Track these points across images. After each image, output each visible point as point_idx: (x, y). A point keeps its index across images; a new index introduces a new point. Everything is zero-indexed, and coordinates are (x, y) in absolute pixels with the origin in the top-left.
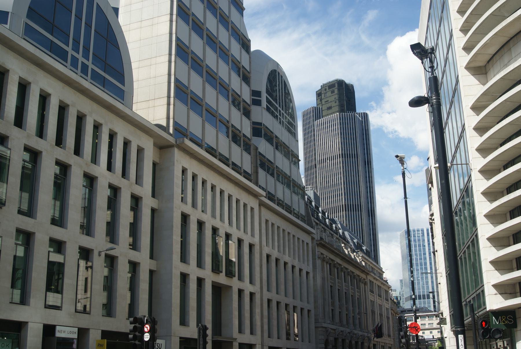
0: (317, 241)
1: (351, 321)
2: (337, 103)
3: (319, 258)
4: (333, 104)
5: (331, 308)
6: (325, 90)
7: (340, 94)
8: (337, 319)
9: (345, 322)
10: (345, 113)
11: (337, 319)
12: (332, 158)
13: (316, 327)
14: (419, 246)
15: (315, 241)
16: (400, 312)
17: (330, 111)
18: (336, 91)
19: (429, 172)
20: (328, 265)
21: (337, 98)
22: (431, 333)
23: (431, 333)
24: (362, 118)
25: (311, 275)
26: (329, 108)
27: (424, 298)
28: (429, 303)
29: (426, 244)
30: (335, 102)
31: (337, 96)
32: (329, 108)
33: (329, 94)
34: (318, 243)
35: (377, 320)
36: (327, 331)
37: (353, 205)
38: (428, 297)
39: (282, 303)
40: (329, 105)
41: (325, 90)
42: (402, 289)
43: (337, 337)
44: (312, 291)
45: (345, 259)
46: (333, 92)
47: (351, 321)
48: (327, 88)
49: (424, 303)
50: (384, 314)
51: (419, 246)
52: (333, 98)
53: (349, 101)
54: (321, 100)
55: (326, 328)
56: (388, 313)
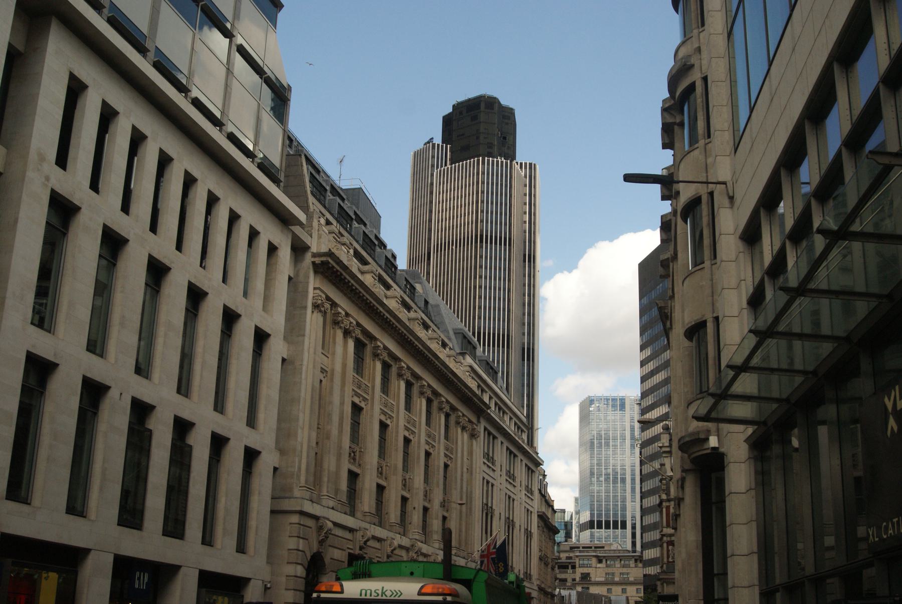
0: (314, 255)
1: (416, 518)
3: (316, 306)
5: (346, 466)
6: (461, 113)
8: (367, 501)
9: (393, 512)
10: (493, 157)
11: (367, 501)
13: (273, 512)
15: (308, 259)
16: (568, 549)
20: (351, 344)
22: (624, 591)
23: (624, 591)
25: (277, 348)
27: (615, 527)
28: (624, 537)
34: (318, 260)
35: (499, 532)
36: (320, 528)
37: (498, 346)
38: (624, 526)
39: (113, 394)
41: (461, 113)
43: (357, 552)
44: (304, 415)
45: (410, 343)
47: (416, 518)
49: (615, 537)
50: (519, 518)
53: (505, 138)
55: (316, 518)
56: (529, 522)
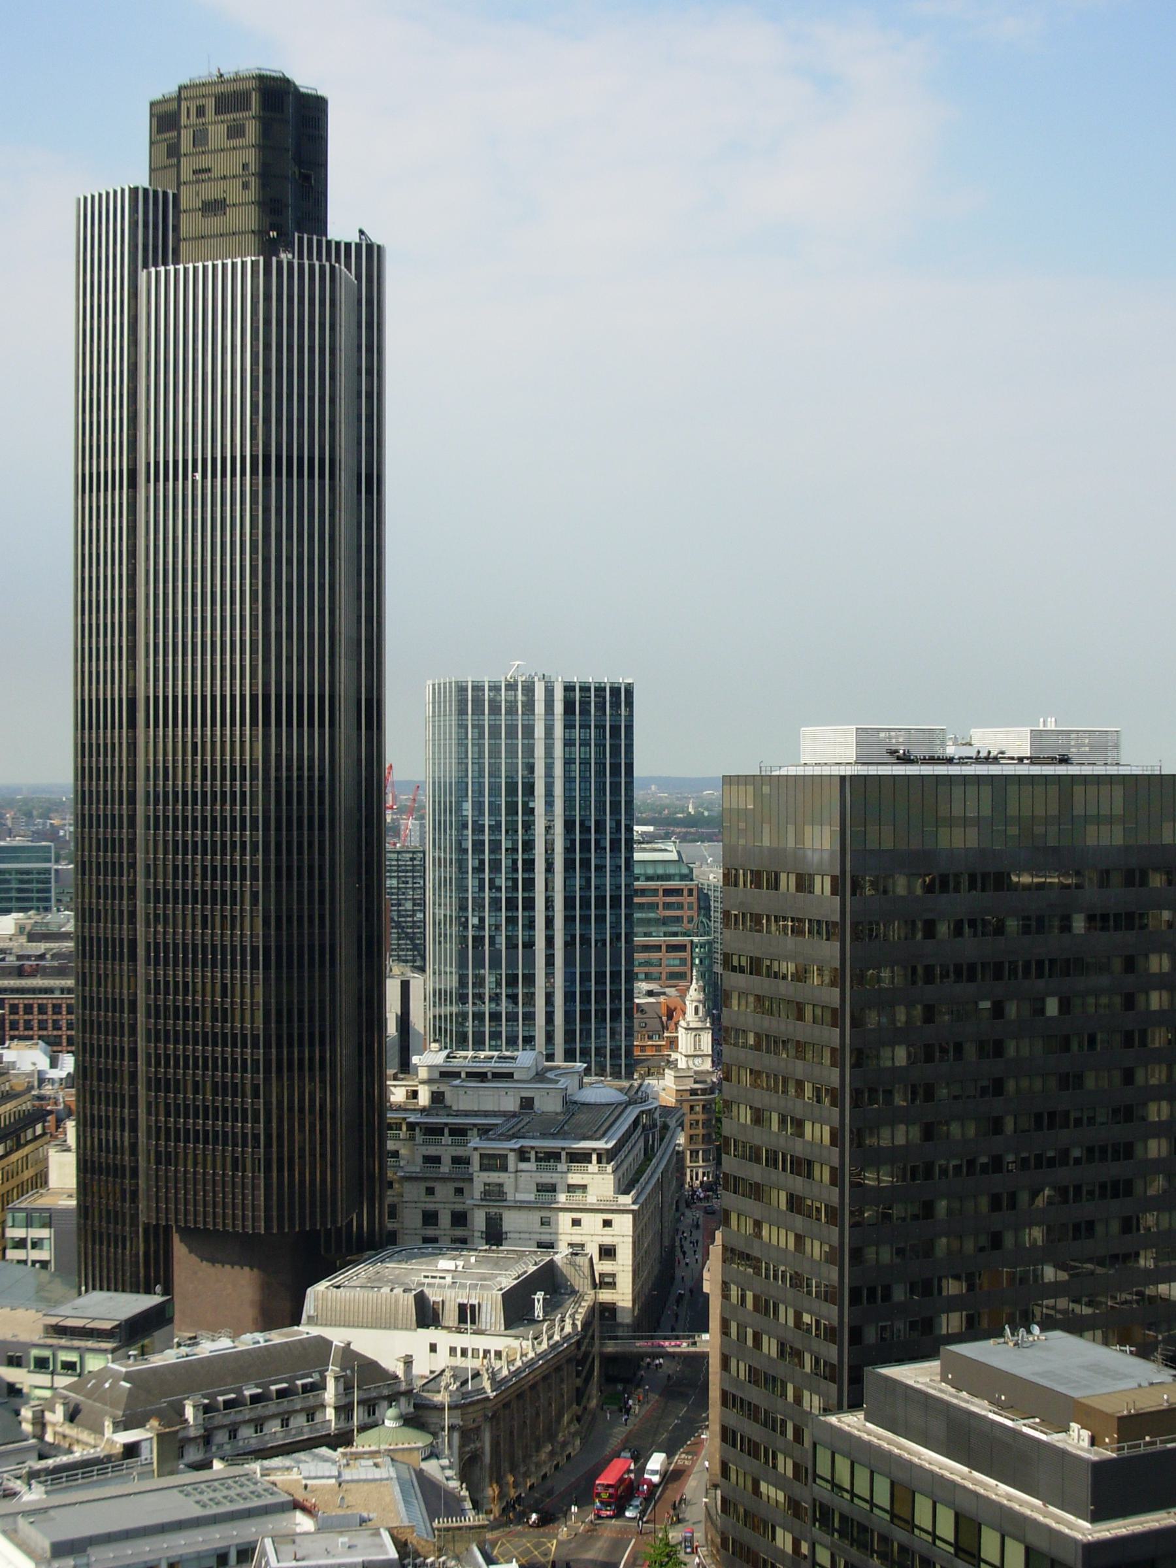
2: (251, 195)
4: (234, 193)
6: (201, 111)
7: (267, 145)
12: (214, 468)
14: (511, 732)
17: (214, 223)
18: (252, 129)
19: (525, 1272)
21: (253, 168)
24: (358, 277)
26: (214, 207)
29: (539, 804)
30: (245, 186)
31: (251, 157)
32: (214, 207)
33: (217, 133)
40: (211, 191)
41: (201, 111)
42: (406, 961)
46: (236, 131)
48: (210, 104)
51: (511, 732)
52: (231, 160)
54: (174, 151)
